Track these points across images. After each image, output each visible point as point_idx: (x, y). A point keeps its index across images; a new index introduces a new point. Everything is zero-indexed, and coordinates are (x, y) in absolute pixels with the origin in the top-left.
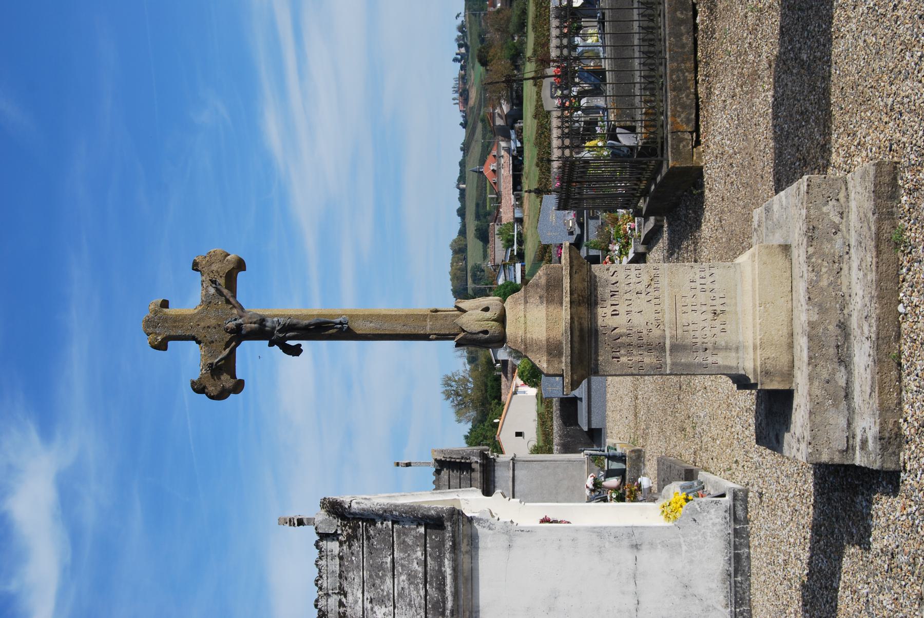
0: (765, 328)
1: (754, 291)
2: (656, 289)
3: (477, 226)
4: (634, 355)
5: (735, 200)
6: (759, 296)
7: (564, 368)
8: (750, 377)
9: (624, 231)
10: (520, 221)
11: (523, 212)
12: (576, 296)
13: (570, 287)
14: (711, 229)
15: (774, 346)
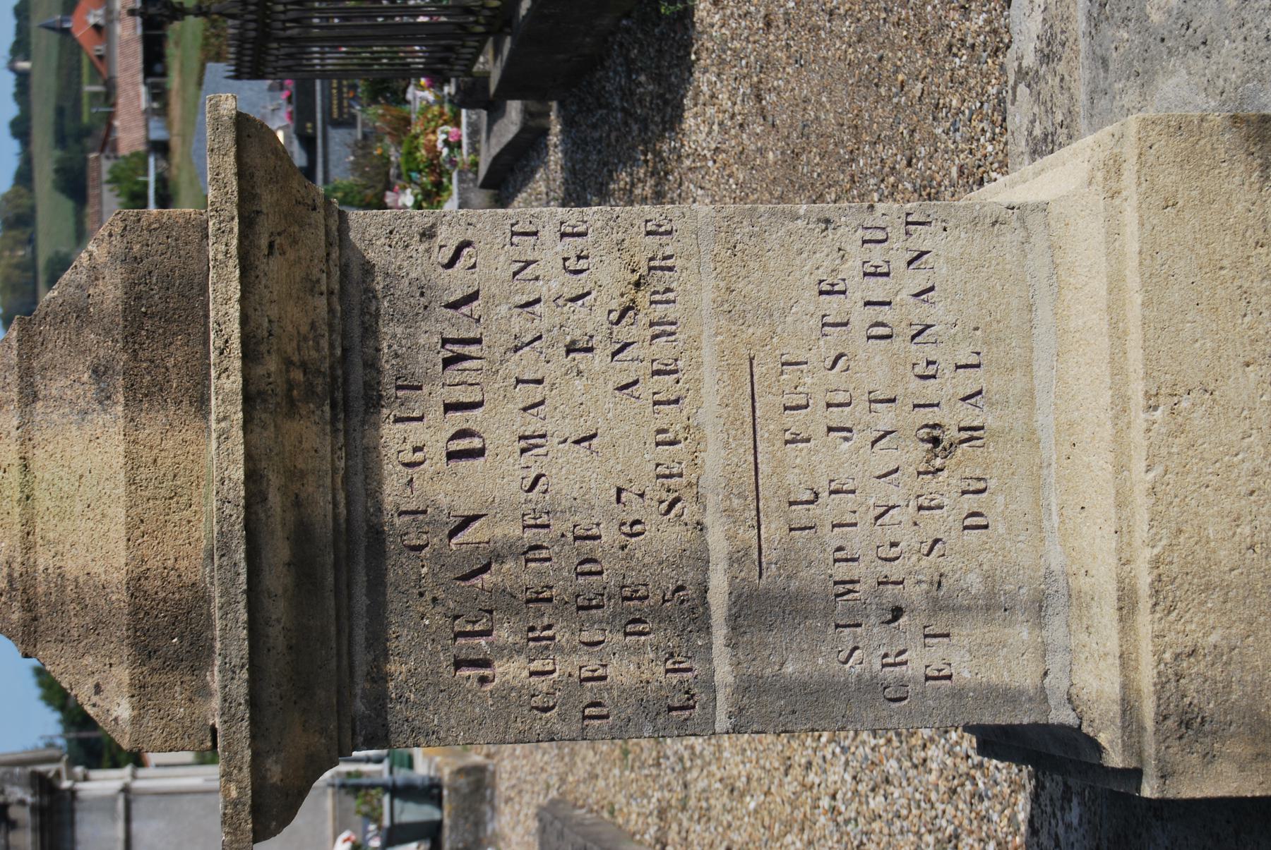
0: (1174, 511)
1: (1117, 333)
2: (662, 329)
3: (58, 161)
4: (560, 650)
5: (821, 20)
6: (1147, 360)
7: (217, 722)
8: (1103, 739)
9: (428, 151)
10: (161, 148)
11: (168, 127)
12: (272, 364)
13: (244, 320)
14: (721, 124)
15: (1217, 595)
